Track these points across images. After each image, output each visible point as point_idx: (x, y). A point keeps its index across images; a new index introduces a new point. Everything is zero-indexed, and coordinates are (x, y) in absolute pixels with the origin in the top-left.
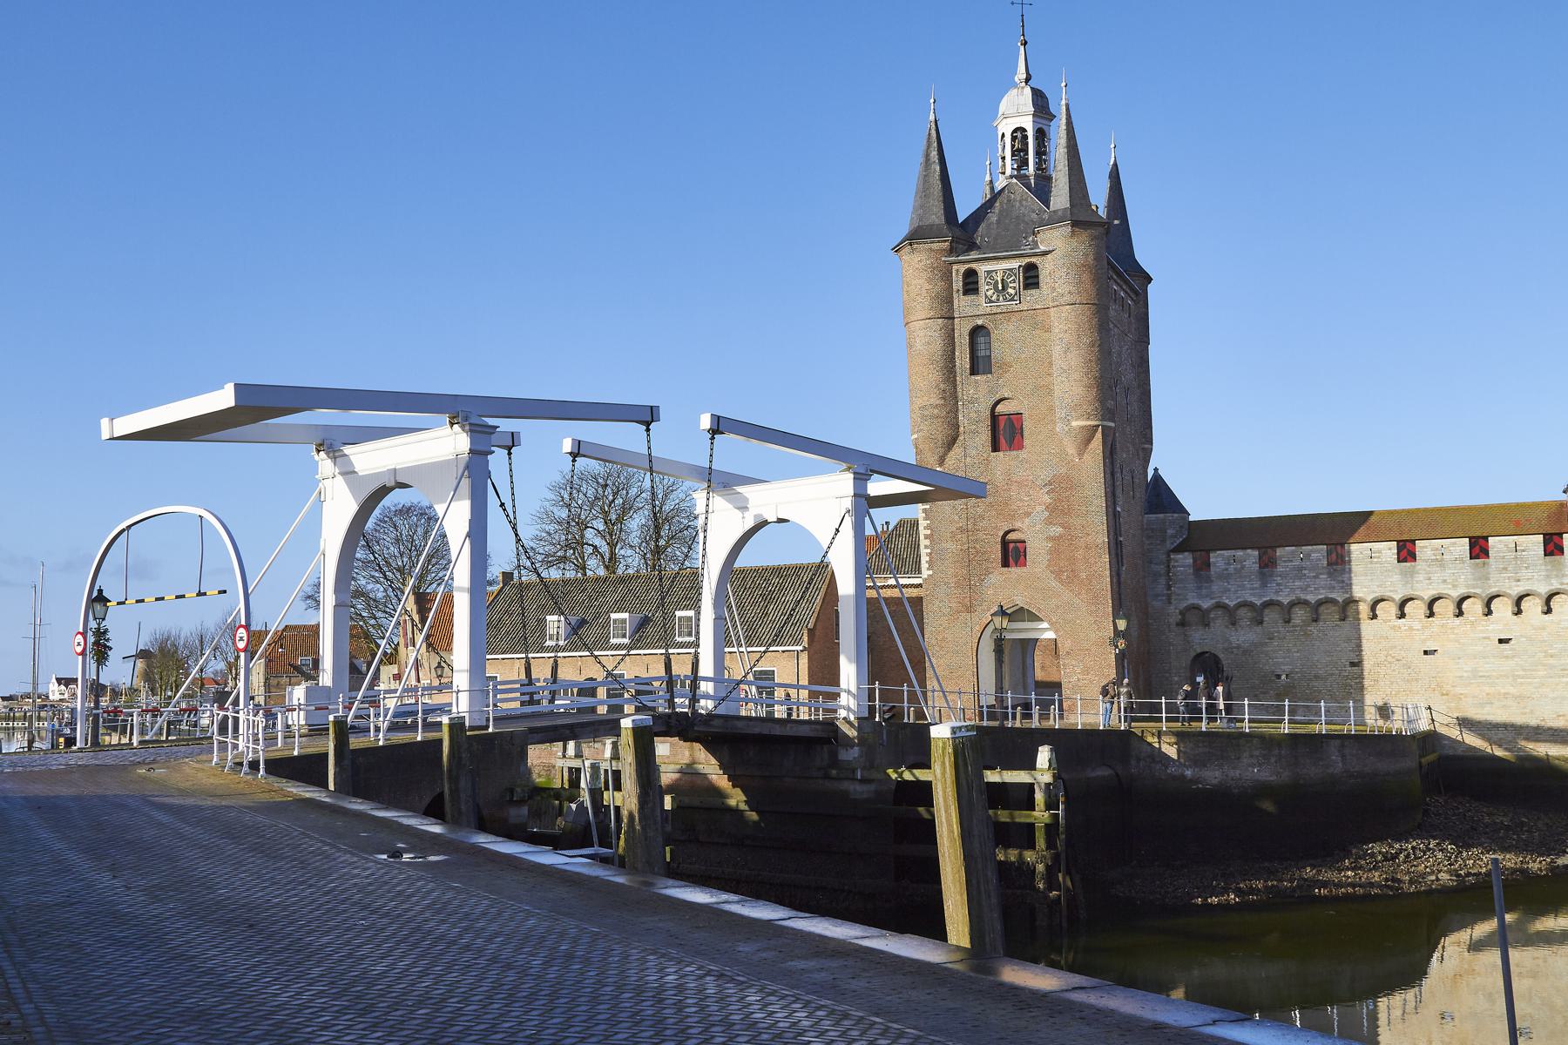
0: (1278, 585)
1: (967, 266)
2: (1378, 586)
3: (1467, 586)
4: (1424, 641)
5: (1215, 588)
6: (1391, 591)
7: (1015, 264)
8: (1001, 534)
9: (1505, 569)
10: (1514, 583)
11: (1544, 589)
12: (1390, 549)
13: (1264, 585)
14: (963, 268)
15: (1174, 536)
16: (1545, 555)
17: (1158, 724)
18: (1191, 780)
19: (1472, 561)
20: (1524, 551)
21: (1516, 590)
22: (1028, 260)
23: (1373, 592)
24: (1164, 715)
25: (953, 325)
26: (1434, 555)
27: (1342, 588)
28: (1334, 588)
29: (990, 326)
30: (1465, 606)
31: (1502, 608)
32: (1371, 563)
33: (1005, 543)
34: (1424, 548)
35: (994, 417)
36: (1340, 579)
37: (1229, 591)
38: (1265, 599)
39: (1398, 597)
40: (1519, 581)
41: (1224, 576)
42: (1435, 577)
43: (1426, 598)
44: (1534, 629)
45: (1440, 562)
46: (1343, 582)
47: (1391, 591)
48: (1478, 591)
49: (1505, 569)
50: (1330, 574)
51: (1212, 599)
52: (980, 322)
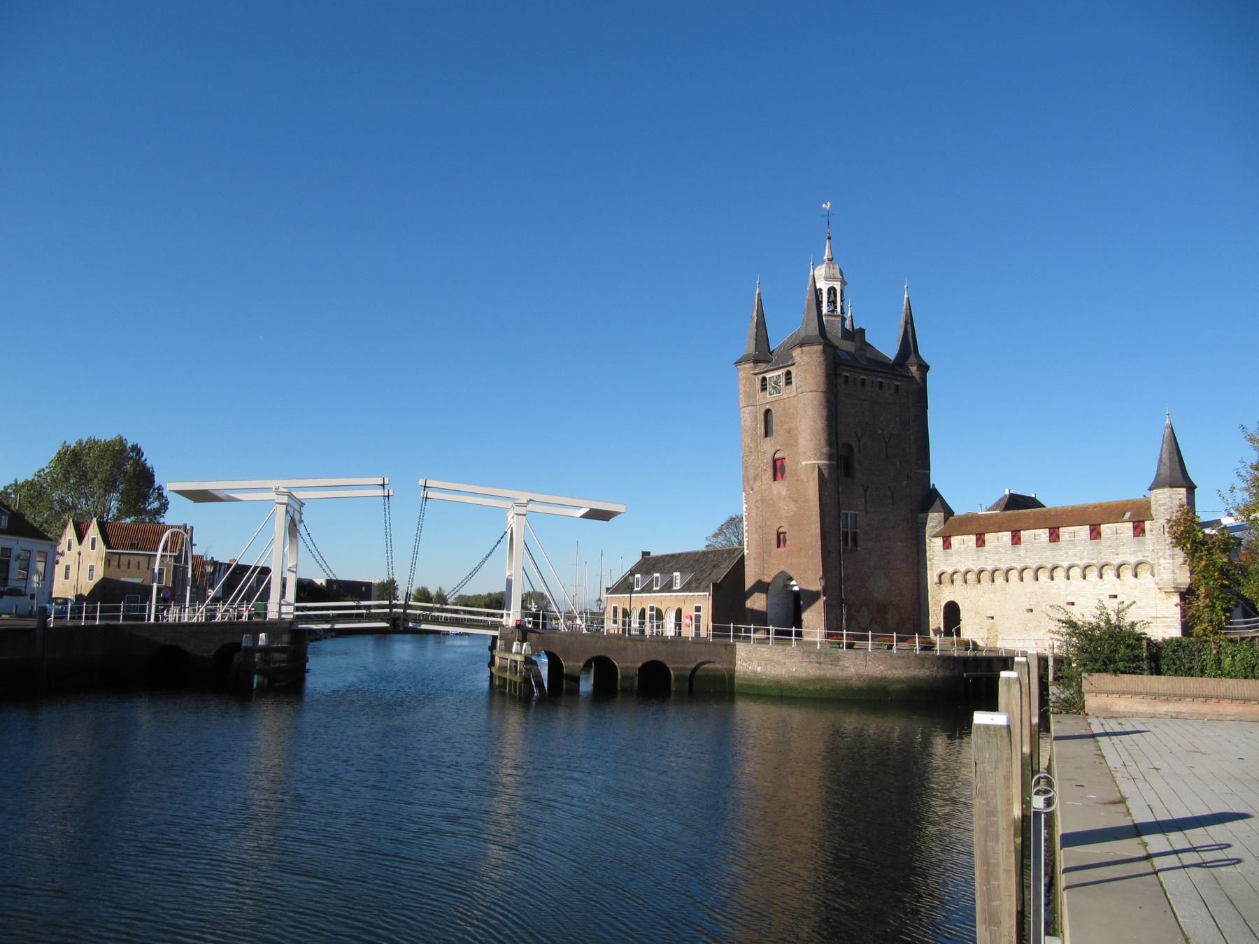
0: (986, 557)
1: (762, 375)
2: (1039, 559)
3: (1088, 558)
4: (1067, 595)
5: (954, 560)
6: (1045, 562)
7: (779, 372)
8: (776, 529)
9: (1110, 546)
10: (1115, 557)
11: (1133, 560)
12: (1045, 533)
13: (978, 558)
14: (760, 377)
15: (933, 527)
16: (1134, 536)
17: (727, 640)
18: (759, 673)
19: (1136, 538)
20: (1121, 533)
21: (1117, 561)
22: (787, 369)
23: (1037, 563)
24: (732, 634)
25: (756, 409)
26: (1070, 537)
27: (1019, 560)
28: (1014, 560)
29: (772, 409)
30: (1087, 571)
31: (1109, 574)
32: (1035, 543)
33: (778, 535)
34: (1065, 532)
35: (775, 461)
36: (1018, 554)
37: (961, 561)
38: (979, 567)
39: (1035, 566)
40: (1118, 554)
41: (959, 553)
42: (1070, 552)
43: (1004, 569)
44: (1131, 588)
45: (1072, 543)
46: (1020, 556)
47: (1045, 562)
48: (1095, 562)
49: (1110, 546)
50: (1013, 551)
51: (953, 567)
52: (768, 407)
